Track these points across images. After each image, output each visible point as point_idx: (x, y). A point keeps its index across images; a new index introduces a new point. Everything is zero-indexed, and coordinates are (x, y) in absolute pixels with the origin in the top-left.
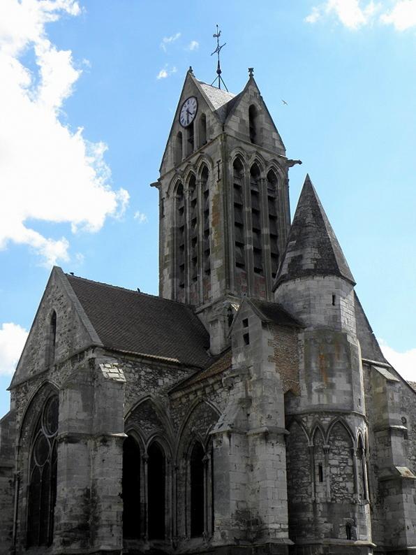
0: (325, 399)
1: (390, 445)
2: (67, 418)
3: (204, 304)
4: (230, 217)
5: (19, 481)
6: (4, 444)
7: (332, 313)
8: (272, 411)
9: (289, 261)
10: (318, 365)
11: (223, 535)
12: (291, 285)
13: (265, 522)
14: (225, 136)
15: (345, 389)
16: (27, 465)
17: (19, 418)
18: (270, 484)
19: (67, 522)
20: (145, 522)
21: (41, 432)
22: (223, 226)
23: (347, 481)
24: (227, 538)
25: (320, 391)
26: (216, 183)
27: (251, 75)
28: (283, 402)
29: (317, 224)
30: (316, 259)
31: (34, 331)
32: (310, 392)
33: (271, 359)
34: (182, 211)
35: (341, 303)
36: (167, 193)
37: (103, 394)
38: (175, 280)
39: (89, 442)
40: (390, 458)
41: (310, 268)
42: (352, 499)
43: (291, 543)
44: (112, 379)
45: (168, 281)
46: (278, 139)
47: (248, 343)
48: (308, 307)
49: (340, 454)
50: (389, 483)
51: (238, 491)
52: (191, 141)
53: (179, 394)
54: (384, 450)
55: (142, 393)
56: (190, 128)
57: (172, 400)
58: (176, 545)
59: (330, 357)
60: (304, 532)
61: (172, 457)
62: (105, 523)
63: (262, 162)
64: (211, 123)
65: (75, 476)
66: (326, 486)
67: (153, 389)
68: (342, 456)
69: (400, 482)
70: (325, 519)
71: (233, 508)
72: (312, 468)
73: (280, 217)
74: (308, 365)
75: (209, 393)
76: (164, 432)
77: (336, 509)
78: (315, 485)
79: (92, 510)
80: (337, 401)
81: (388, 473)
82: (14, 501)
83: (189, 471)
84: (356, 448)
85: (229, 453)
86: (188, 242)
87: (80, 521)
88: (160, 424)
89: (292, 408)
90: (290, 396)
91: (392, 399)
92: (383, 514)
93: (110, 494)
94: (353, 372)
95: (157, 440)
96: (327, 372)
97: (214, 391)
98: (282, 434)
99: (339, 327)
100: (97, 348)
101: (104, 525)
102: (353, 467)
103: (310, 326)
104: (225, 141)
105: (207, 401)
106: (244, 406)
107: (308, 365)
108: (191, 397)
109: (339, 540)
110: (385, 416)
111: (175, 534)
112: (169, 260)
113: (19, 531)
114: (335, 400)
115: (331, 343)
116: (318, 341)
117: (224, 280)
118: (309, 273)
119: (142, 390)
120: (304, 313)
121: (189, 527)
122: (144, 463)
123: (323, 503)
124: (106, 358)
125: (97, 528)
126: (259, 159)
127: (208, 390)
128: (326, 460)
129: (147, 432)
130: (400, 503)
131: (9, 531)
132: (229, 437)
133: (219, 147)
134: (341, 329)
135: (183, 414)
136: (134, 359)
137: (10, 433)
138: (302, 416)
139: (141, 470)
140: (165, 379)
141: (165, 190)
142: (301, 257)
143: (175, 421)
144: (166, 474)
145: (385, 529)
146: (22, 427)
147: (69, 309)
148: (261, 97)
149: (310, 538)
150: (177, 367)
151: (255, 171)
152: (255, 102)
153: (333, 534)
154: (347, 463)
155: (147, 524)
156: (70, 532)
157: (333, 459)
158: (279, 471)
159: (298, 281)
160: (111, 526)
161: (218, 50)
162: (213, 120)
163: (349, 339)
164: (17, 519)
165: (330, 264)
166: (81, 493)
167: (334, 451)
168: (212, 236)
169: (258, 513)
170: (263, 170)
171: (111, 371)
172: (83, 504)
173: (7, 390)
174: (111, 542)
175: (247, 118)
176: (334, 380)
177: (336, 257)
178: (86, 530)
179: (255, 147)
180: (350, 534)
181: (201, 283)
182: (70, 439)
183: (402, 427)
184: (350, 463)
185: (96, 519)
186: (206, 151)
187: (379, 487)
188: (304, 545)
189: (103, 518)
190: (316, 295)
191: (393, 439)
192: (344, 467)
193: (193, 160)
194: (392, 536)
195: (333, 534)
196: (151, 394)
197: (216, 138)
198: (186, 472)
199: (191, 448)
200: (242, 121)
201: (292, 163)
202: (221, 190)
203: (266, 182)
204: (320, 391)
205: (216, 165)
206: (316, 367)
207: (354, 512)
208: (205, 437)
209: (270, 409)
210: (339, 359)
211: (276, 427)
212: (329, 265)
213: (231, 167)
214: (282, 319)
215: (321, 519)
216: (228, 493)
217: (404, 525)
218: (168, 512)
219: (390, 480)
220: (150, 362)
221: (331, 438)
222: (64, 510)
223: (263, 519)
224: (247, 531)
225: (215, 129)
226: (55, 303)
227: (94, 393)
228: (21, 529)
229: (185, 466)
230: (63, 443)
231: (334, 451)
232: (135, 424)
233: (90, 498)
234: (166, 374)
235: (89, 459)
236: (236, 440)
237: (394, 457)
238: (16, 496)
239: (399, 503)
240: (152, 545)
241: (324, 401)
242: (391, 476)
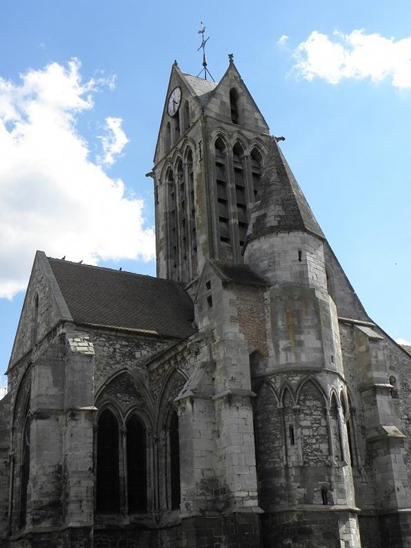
0: (293, 357)
1: (376, 404)
2: (36, 394)
3: (193, 279)
4: (213, 193)
7: (298, 269)
8: (236, 373)
11: (187, 506)
13: (232, 490)
14: (205, 118)
15: (315, 346)
17: (13, 400)
18: (235, 449)
19: (37, 499)
22: (205, 202)
24: (192, 509)
25: (287, 349)
26: (199, 163)
27: (231, 61)
28: (249, 363)
29: (281, 181)
31: (23, 315)
32: (277, 352)
34: (173, 196)
35: (308, 258)
36: (160, 180)
37: (72, 368)
39: (60, 417)
40: (376, 417)
41: (273, 225)
42: (327, 462)
43: (261, 511)
44: (79, 352)
45: (163, 263)
47: (211, 306)
48: (273, 264)
49: (311, 414)
50: (377, 444)
51: (203, 458)
52: (178, 129)
53: (155, 366)
54: (371, 409)
56: (176, 116)
57: (151, 372)
58: (158, 518)
59: (298, 314)
61: (152, 430)
62: (73, 499)
63: (244, 140)
65: (45, 452)
66: (297, 449)
67: (129, 362)
69: (389, 442)
70: (298, 484)
71: (198, 476)
74: (274, 324)
75: (180, 361)
76: (144, 404)
78: (286, 449)
79: (64, 486)
80: (306, 358)
81: (376, 434)
83: (168, 442)
84: (329, 406)
85: (194, 419)
86: (179, 223)
87: (51, 498)
88: (139, 396)
89: (261, 369)
90: (256, 357)
91: (376, 357)
92: (373, 476)
93: (80, 470)
94: (323, 328)
95: (137, 413)
96: (295, 329)
97: (183, 359)
98: (247, 396)
99: (306, 283)
100: (66, 323)
101: (73, 501)
102: (327, 427)
103: (275, 284)
104: (205, 122)
106: (208, 370)
107: (274, 324)
108: (166, 367)
109: (312, 506)
110: (369, 375)
111: (157, 507)
112: (164, 243)
114: (304, 358)
115: (298, 299)
116: (284, 298)
118: (273, 230)
119: (118, 363)
121: (170, 499)
124: (76, 333)
125: (67, 504)
126: (241, 137)
127: (179, 358)
128: (297, 421)
129: (124, 406)
130: (388, 463)
131: (5, 511)
132: (192, 402)
133: (200, 129)
134: (308, 284)
135: (161, 385)
136: (108, 333)
137: (5, 415)
138: (270, 377)
139: (120, 444)
140: (143, 351)
141: (158, 178)
142: (265, 216)
144: (132, 446)
145: (376, 492)
146: (15, 409)
147: (47, 289)
148: (242, 80)
149: (283, 505)
150: (156, 339)
151: (237, 150)
152: (236, 85)
153: (307, 500)
154: (320, 423)
155: (127, 498)
156: (40, 509)
157: (304, 420)
159: (262, 239)
160: (81, 501)
161: (203, 45)
162: (194, 104)
163: (318, 294)
165: (295, 218)
166: (52, 469)
167: (304, 412)
168: (197, 214)
169: (225, 481)
170: (246, 149)
171: (80, 344)
172: (54, 480)
173: (5, 374)
174: (80, 519)
175: (227, 100)
176: (302, 337)
177: (302, 213)
178: (57, 506)
179: (237, 126)
181: (190, 260)
182: (41, 415)
183: (389, 385)
184: (323, 422)
185: (67, 495)
187: (367, 449)
188: (277, 513)
189: (71, 494)
190: (280, 252)
191: (379, 398)
192: (317, 428)
193: (179, 146)
194: (383, 499)
195: (307, 500)
196: (128, 367)
197: (197, 121)
198: (166, 444)
199: (170, 418)
200: (223, 103)
202: (203, 168)
203: (250, 159)
204: (287, 349)
205: (198, 146)
206: (283, 325)
207: (329, 475)
209: (233, 371)
210: (307, 316)
211: (242, 390)
212: (293, 221)
213: (212, 147)
214: (245, 279)
215: (293, 484)
216: (192, 461)
217: (394, 486)
218: (150, 485)
219: (378, 440)
220: (124, 335)
221: (302, 398)
222: (34, 487)
223: (230, 487)
224: (215, 501)
225: (196, 112)
226: (38, 285)
227: (65, 368)
228: (16, 509)
229: (164, 436)
230: (34, 420)
231: (304, 412)
232: (112, 397)
233: (60, 474)
234: (144, 347)
235: (61, 435)
236: (199, 405)
237: (380, 416)
238: (11, 477)
240: (133, 519)
241: (292, 360)
242: (378, 436)
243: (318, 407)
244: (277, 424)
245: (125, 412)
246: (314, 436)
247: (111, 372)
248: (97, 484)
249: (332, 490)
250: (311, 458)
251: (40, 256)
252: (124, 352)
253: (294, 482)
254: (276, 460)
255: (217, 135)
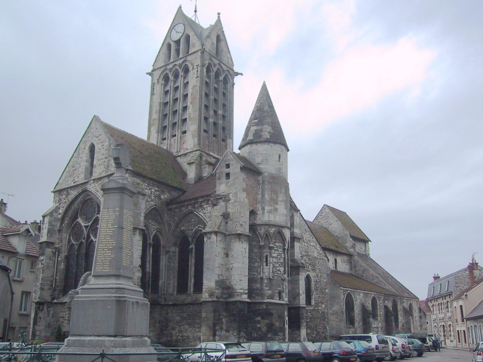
5: (58, 252)
6: (50, 227)
9: (254, 132)
10: (269, 197)
12: (254, 146)
14: (203, 51)
16: (65, 242)
17: (61, 211)
20: (149, 284)
21: (77, 222)
23: (281, 267)
27: (219, 17)
30: (271, 133)
32: (263, 213)
33: (244, 190)
38: (159, 134)
46: (230, 58)
49: (278, 250)
51: (219, 268)
52: (178, 51)
55: (152, 203)
56: (178, 42)
60: (254, 295)
63: (221, 70)
64: (194, 41)
68: (279, 252)
70: (268, 288)
72: (261, 259)
73: (228, 105)
77: (274, 282)
82: (54, 265)
83: (177, 254)
90: (253, 213)
97: (201, 206)
102: (284, 258)
105: (196, 212)
112: (156, 122)
113: (57, 283)
117: (197, 138)
119: (152, 201)
120: (262, 164)
122: (150, 246)
123: (267, 279)
126: (220, 68)
128: (271, 253)
143: (169, 222)
151: (217, 75)
152: (221, 34)
154: (281, 256)
155: (150, 285)
157: (274, 253)
158: (245, 258)
164: (56, 276)
167: (275, 248)
176: (278, 207)
180: (280, 297)
186: (189, 58)
192: (280, 258)
199: (180, 240)
201: (237, 74)
204: (270, 212)
205: (195, 67)
206: (268, 197)
208: (191, 234)
213: (205, 70)
215: (265, 288)
226: (95, 138)
239: (297, 280)
243: (281, 247)
244: (258, 254)
245: (152, 231)
246: (278, 263)
247: (148, 206)
248: (311, 298)
249: (283, 293)
250: (275, 274)
251: (96, 119)
252: (155, 194)
253: (265, 286)
254: (254, 273)
255: (208, 64)
